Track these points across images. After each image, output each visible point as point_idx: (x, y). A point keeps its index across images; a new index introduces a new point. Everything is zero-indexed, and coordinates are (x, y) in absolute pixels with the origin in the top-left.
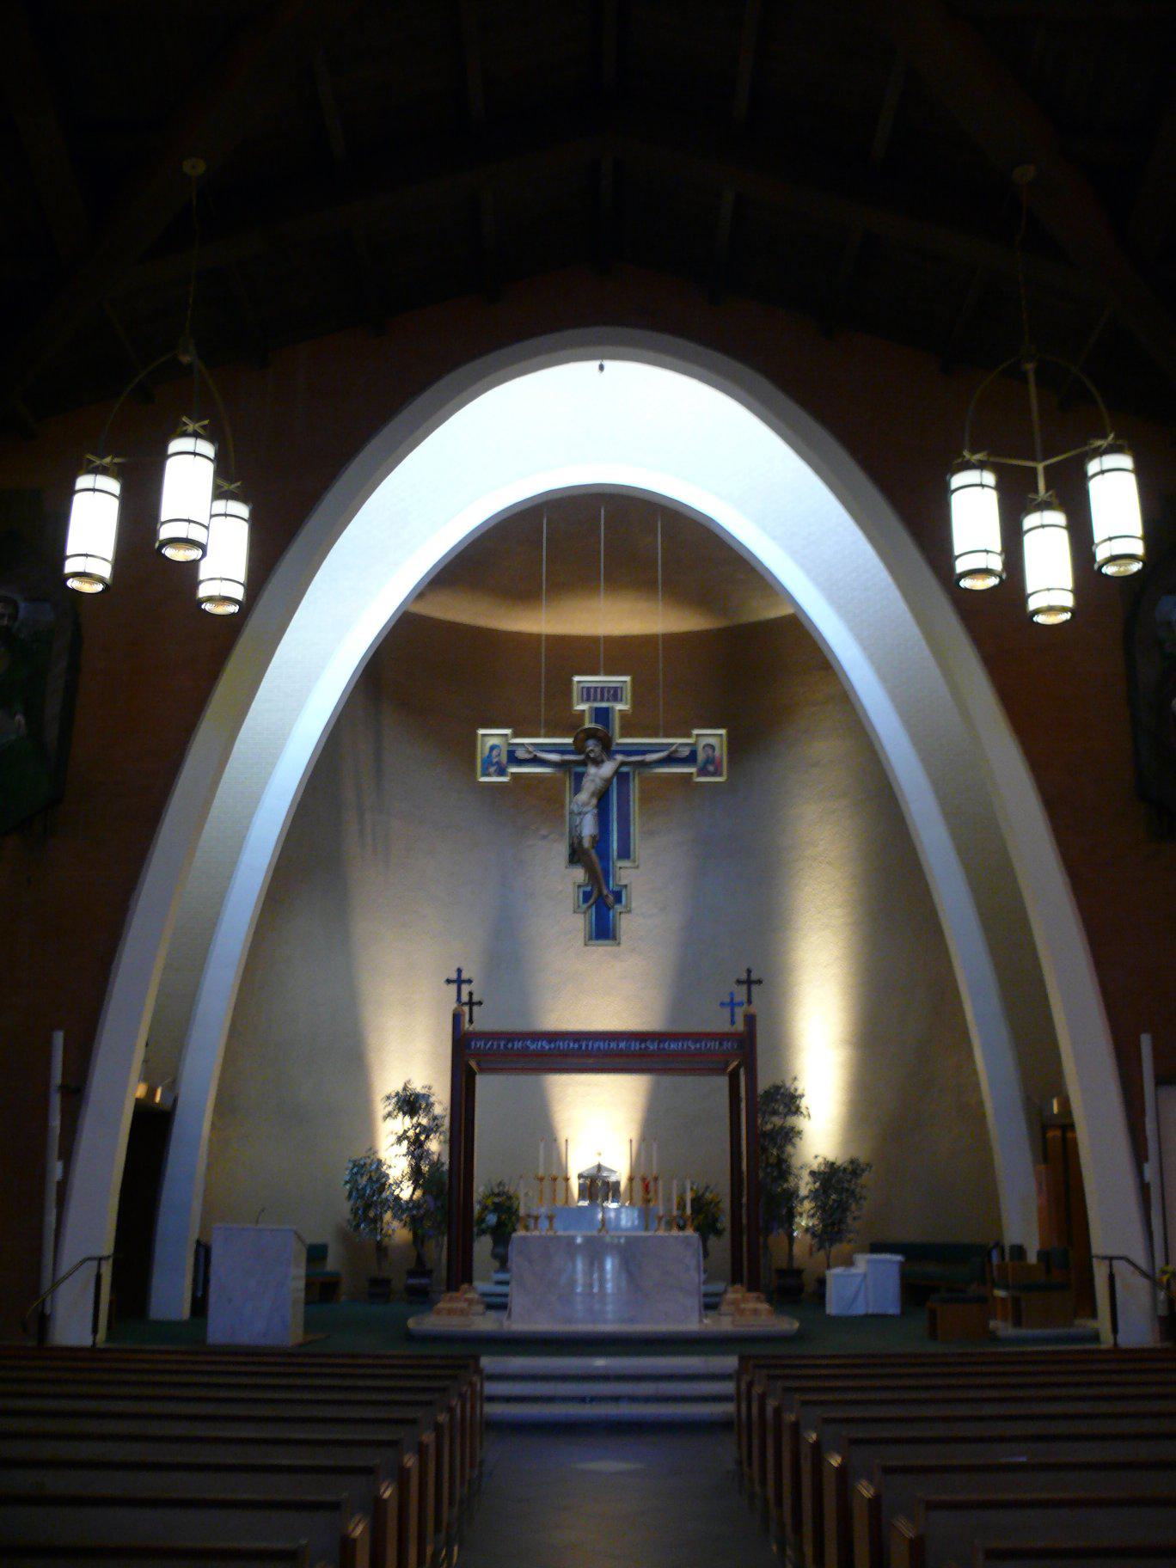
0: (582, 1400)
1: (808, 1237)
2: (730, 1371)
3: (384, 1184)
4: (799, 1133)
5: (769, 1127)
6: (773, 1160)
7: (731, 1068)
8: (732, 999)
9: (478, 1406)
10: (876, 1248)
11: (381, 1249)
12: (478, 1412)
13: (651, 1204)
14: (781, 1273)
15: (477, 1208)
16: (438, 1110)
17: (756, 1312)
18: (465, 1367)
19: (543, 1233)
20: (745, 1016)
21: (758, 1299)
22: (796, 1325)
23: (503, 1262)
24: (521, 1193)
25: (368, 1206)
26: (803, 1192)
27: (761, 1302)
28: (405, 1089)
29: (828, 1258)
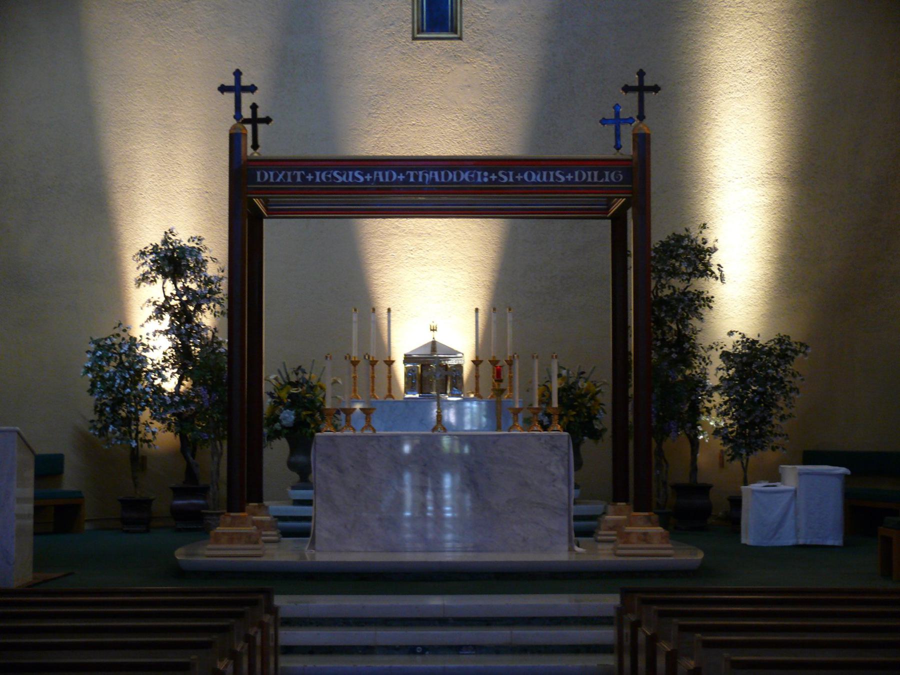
0: (411, 650)
1: (719, 440)
2: (612, 613)
3: (141, 371)
4: (709, 300)
5: (667, 292)
6: (671, 338)
7: (614, 209)
8: (617, 114)
9: (272, 659)
10: (810, 458)
11: (137, 460)
12: (272, 666)
13: (505, 397)
14: (679, 489)
15: (267, 401)
16: (212, 270)
17: (645, 538)
18: (254, 603)
19: (358, 433)
20: (635, 135)
21: (649, 521)
22: (700, 556)
23: (304, 474)
24: (327, 384)
25: (118, 402)
26: (713, 380)
27: (653, 525)
28: (165, 242)
29: (745, 469)
